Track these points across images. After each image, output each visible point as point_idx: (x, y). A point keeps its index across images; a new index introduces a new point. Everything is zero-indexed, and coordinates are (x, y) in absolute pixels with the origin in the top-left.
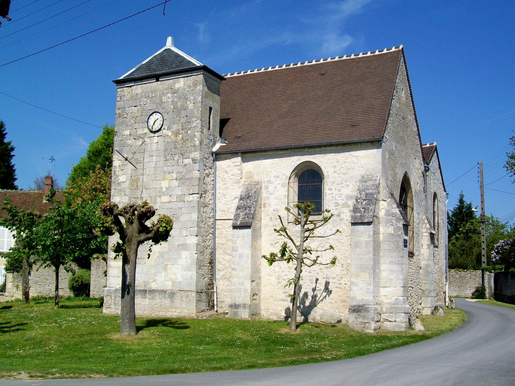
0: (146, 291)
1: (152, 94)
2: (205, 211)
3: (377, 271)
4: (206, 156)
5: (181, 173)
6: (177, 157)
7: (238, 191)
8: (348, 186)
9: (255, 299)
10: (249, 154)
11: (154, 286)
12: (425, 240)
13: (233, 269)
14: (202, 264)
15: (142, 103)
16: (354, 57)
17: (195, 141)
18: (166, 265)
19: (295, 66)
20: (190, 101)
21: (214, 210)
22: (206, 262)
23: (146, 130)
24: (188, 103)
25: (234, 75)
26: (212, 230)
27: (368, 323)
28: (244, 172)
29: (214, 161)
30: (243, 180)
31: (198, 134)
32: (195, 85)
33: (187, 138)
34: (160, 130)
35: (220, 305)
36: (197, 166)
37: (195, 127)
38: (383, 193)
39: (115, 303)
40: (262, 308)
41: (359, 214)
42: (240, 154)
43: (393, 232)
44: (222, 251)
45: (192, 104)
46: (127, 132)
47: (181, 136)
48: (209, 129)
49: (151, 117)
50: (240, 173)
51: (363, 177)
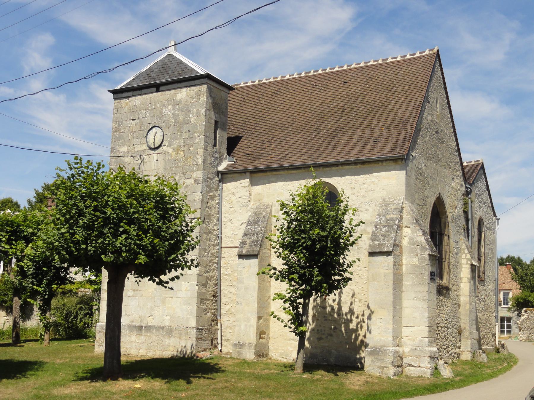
0: (142, 327)
1: (152, 105)
2: (208, 237)
3: (398, 307)
7: (246, 216)
9: (263, 338)
10: (259, 174)
11: (151, 322)
12: (465, 273)
13: (238, 303)
14: (204, 298)
15: (140, 116)
17: (197, 159)
18: (165, 298)
19: (315, 73)
20: (193, 114)
21: (219, 237)
22: (209, 296)
23: (145, 147)
24: (191, 116)
26: (217, 259)
27: (386, 367)
28: (253, 194)
29: (220, 181)
30: (252, 203)
31: (201, 151)
32: (199, 95)
34: (160, 146)
35: (224, 343)
36: (199, 187)
37: (197, 143)
38: (407, 218)
40: (271, 348)
41: (377, 243)
42: (248, 174)
43: (417, 263)
44: (227, 283)
46: (124, 149)
47: (182, 153)
48: (215, 145)
49: (150, 132)
50: (248, 195)
51: (384, 200)
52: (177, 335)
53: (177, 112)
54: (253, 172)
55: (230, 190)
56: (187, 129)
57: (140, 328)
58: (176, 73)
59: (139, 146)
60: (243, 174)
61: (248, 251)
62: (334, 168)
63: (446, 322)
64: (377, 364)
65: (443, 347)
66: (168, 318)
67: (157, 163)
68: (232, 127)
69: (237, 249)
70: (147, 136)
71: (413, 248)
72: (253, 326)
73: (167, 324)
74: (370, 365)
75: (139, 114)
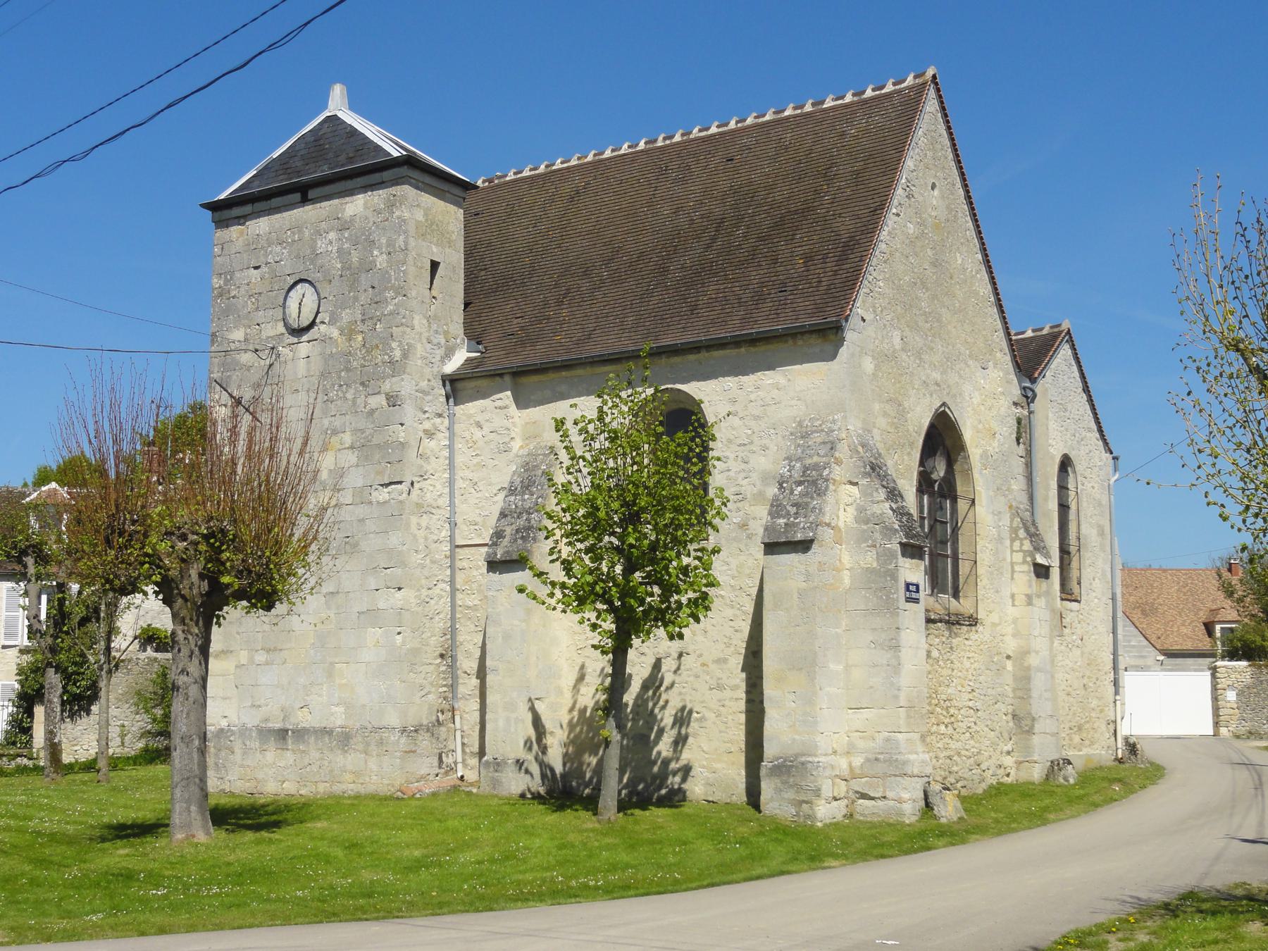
0: (287, 731)
1: (294, 233)
2: (424, 524)
4: (424, 384)
5: (362, 431)
6: (352, 391)
8: (765, 448)
11: (304, 719)
16: (832, 104)
17: (392, 349)
18: (332, 664)
19: (668, 142)
20: (379, 248)
23: (281, 328)
25: (524, 174)
33: (375, 342)
37: (391, 314)
39: (216, 764)
41: (782, 521)
42: (507, 379)
43: (875, 565)
44: (472, 626)
45: (384, 256)
46: (238, 335)
47: (360, 338)
49: (291, 294)
51: (800, 424)
52: (361, 747)
53: (346, 246)
54: (518, 374)
55: (470, 416)
56: (369, 284)
57: (282, 734)
58: (342, 158)
59: (269, 326)
60: (498, 378)
61: (507, 552)
62: (692, 357)
63: (970, 696)
64: (786, 796)
65: (964, 752)
66: (341, 709)
67: (308, 363)
68: (483, 273)
69: (485, 549)
70: (284, 303)
71: (865, 531)
72: (523, 721)
73: (339, 723)
74: (772, 799)
75: (266, 255)
